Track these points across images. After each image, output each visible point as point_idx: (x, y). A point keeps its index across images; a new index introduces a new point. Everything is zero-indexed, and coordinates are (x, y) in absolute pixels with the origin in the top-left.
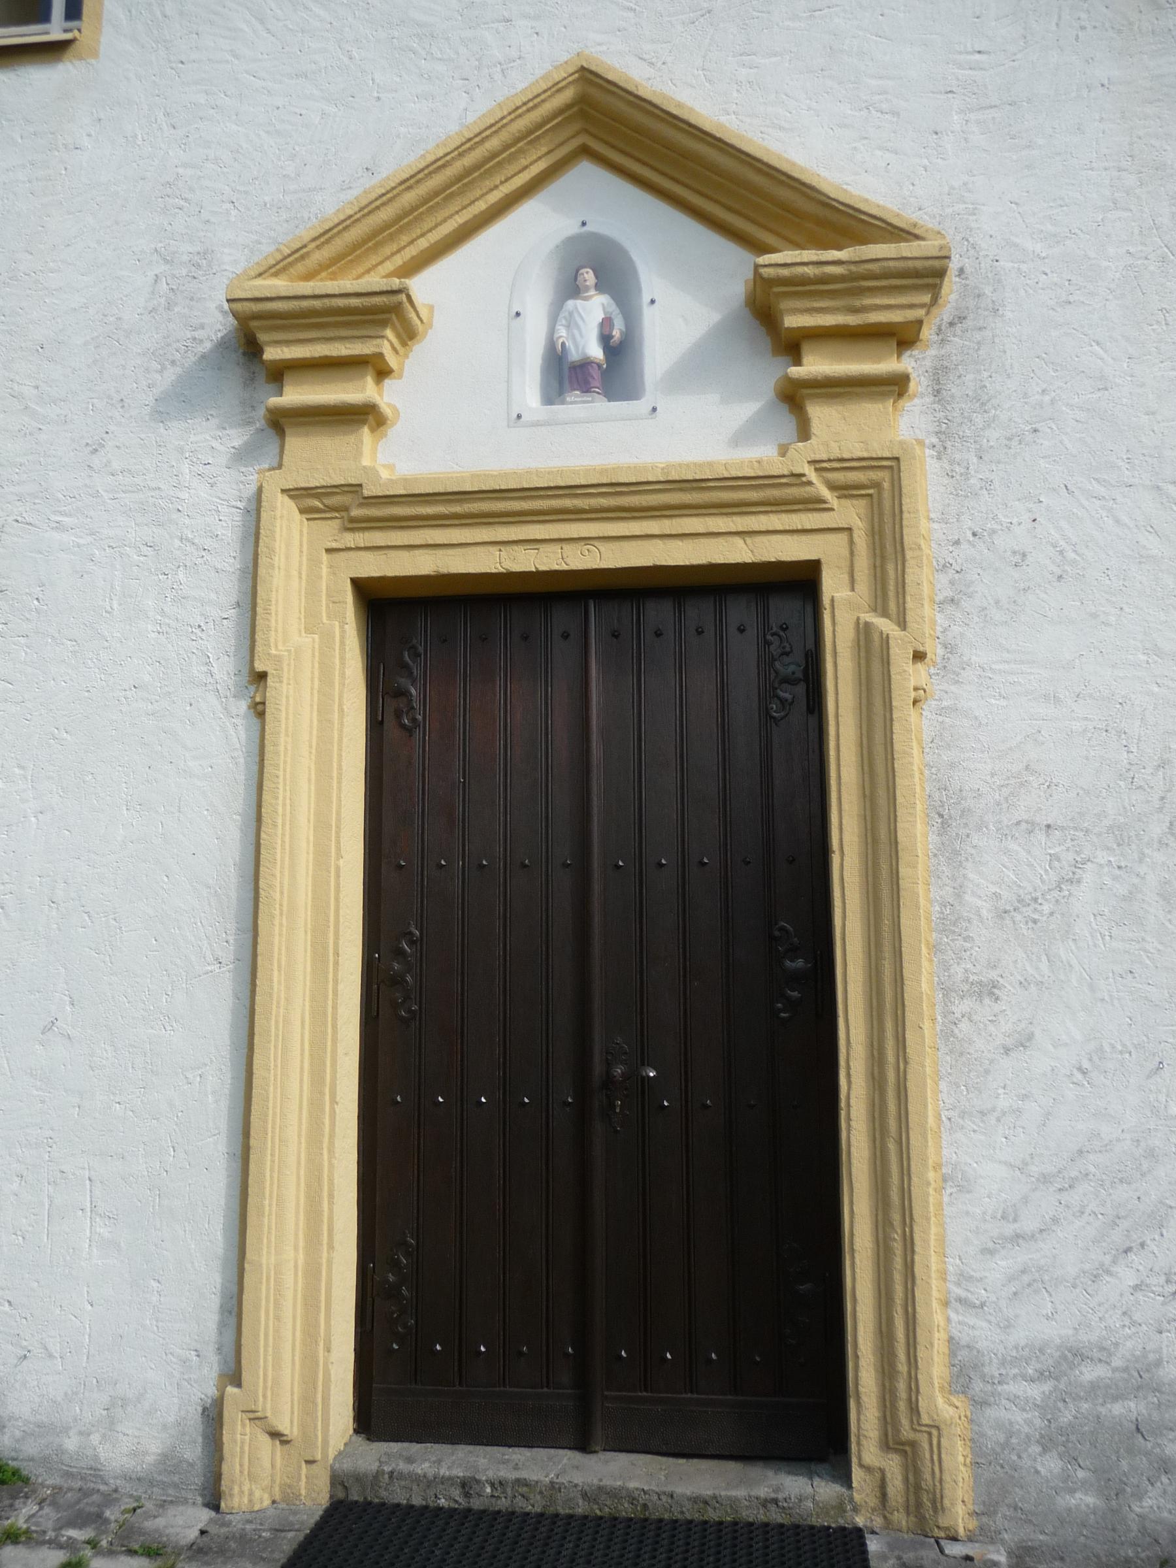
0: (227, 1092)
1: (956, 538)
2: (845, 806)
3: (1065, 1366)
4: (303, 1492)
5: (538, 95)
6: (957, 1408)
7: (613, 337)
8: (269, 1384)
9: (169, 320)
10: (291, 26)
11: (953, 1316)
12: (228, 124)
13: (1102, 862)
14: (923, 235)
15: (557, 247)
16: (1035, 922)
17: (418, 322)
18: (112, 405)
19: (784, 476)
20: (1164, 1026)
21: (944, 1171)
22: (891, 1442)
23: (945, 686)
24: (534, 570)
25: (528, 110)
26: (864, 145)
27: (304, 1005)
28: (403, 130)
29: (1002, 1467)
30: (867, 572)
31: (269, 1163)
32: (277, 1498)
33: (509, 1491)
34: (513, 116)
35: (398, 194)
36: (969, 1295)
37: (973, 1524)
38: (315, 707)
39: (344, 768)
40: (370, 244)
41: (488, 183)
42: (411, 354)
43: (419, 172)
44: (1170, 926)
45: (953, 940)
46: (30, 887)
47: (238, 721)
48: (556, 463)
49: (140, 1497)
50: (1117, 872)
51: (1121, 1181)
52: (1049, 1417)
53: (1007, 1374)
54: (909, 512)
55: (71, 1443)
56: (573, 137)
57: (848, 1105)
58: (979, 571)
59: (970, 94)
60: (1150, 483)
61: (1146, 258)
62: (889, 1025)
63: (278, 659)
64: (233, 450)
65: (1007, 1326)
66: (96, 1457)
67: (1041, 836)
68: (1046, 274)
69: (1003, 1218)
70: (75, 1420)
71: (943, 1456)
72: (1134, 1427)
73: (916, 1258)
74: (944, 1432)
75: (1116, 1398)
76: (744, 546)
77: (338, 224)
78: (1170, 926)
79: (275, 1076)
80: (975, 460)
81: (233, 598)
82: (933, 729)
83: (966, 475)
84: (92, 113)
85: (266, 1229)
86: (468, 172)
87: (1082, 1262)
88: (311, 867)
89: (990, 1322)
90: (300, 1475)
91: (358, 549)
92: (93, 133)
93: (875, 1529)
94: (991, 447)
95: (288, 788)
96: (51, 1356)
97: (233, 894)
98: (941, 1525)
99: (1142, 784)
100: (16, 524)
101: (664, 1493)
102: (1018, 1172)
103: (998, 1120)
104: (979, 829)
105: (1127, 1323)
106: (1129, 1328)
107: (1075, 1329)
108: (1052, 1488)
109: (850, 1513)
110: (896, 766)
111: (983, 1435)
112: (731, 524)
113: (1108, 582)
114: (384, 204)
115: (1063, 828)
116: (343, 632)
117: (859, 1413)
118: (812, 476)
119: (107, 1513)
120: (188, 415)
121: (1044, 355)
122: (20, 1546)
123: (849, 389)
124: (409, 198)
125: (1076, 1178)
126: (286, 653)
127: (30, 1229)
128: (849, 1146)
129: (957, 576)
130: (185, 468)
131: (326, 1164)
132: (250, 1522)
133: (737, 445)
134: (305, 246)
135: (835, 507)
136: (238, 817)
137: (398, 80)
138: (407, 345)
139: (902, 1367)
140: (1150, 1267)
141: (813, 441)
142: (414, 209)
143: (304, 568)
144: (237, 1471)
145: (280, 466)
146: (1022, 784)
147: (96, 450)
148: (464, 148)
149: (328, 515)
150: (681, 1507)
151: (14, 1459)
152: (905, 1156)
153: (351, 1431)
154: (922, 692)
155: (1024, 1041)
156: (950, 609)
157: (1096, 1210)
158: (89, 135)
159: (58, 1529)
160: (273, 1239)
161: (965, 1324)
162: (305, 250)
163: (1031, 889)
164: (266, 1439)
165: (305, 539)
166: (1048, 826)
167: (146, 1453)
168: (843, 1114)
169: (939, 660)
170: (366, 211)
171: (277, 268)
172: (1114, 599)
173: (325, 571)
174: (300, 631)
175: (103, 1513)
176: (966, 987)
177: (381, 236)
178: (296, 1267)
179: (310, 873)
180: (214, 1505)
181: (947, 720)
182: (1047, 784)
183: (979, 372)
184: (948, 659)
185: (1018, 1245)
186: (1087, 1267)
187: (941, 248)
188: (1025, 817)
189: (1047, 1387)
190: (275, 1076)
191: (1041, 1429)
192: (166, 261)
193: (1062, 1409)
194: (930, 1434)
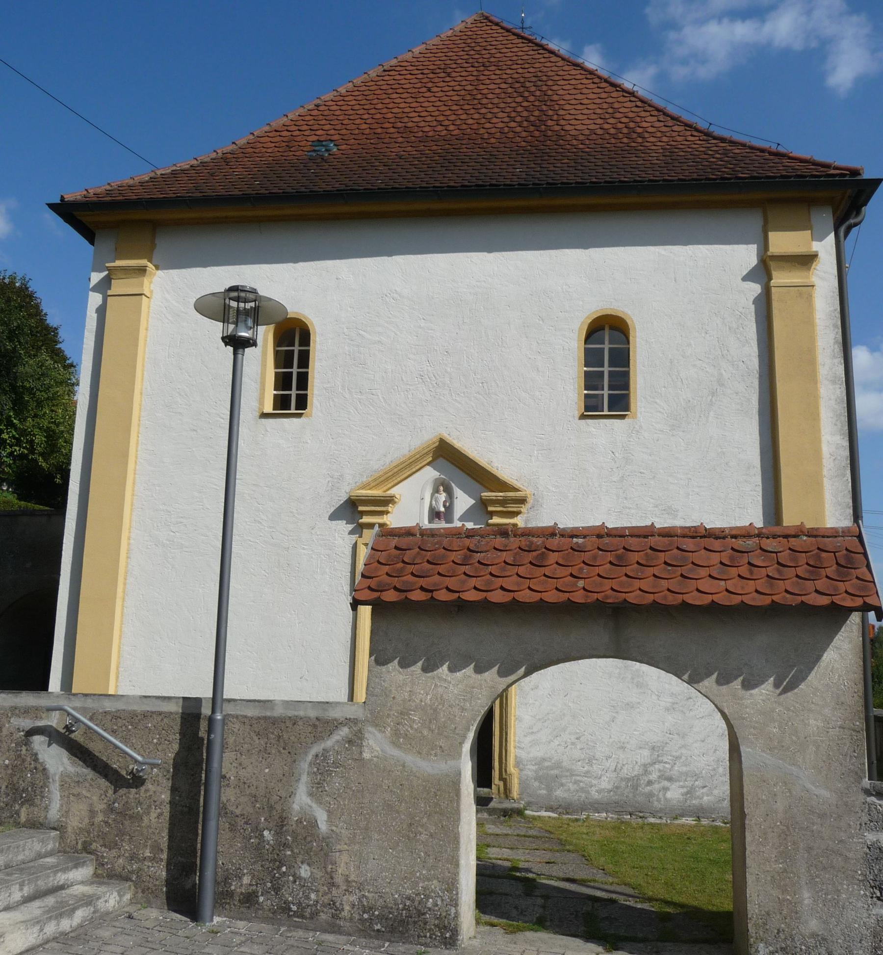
37: (518, 796)
65: (529, 753)
124: (396, 470)
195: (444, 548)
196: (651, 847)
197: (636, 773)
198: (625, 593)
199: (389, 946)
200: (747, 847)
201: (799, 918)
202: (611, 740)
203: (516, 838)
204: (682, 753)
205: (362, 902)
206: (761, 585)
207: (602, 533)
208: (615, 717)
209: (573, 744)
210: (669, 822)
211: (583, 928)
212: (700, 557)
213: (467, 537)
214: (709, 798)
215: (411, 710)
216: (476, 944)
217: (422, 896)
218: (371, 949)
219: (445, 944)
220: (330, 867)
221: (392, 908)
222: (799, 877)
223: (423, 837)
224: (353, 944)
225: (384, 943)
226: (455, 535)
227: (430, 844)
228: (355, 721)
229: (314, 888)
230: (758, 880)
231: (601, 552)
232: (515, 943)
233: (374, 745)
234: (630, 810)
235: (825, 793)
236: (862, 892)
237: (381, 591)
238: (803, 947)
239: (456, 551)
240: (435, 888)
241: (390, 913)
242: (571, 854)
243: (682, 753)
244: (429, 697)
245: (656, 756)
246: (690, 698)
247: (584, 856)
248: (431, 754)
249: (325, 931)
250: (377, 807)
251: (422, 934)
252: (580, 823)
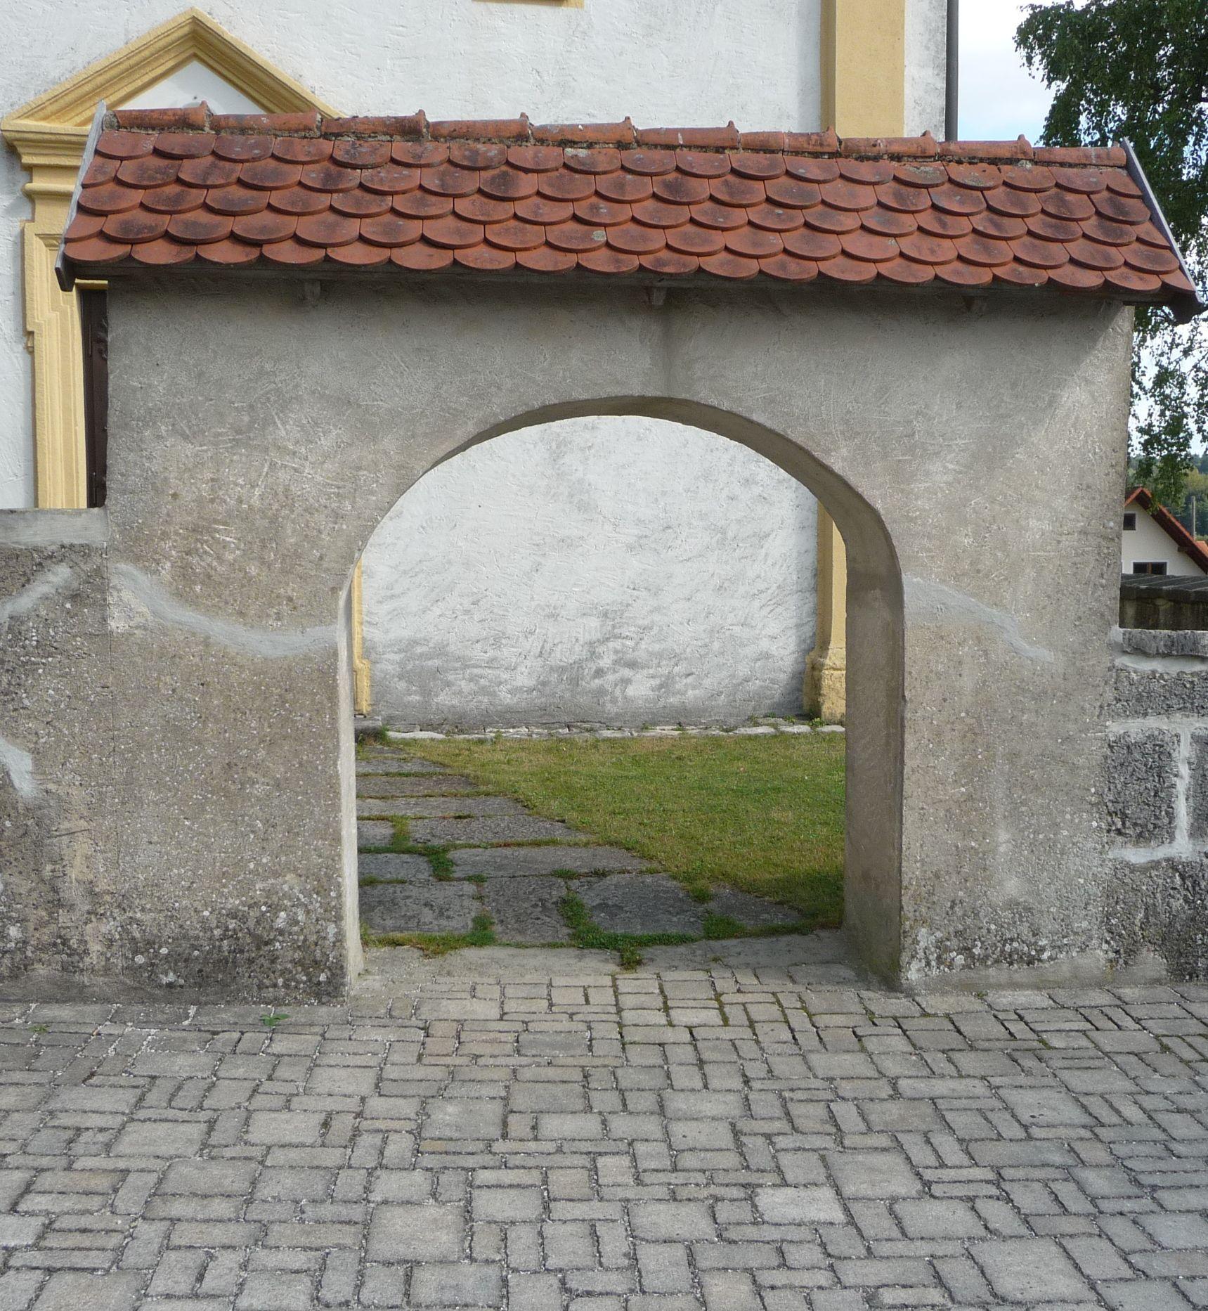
37: (369, 709)
63: (39, 325)
65: (387, 632)
81: (11, 290)
86: (131, 67)
116: (72, 310)
124: (100, 80)
145: (33, 220)
189: (402, 655)
195: (273, 156)
196: (627, 777)
197: (576, 657)
198: (699, 255)
199: (197, 1013)
200: (906, 760)
201: (989, 878)
202: (533, 604)
203: (384, 779)
204: (653, 622)
205: (128, 932)
206: (967, 247)
207: (629, 137)
208: (540, 564)
209: (467, 612)
210: (635, 734)
211: (566, 931)
212: (837, 192)
213: (326, 136)
214: (697, 692)
215: (218, 522)
216: (377, 985)
217: (264, 908)
218: (161, 1025)
219: (318, 996)
220: (49, 867)
221: (197, 938)
222: (993, 807)
223: (259, 790)
224: (116, 1018)
225: (186, 1010)
226: (297, 131)
227: (276, 802)
228: (85, 551)
229: (14, 914)
230: (922, 818)
231: (629, 177)
232: (449, 974)
233: (134, 603)
234: (566, 719)
235: (1046, 655)
236: (1095, 824)
237: (133, 243)
238: (993, 927)
239: (303, 163)
240: (291, 888)
241: (194, 948)
242: (491, 800)
243: (653, 622)
244: (257, 492)
245: (609, 628)
246: (669, 527)
247: (517, 800)
248: (268, 616)
249: (47, 1000)
250: (150, 735)
251: (267, 982)
252: (488, 746)
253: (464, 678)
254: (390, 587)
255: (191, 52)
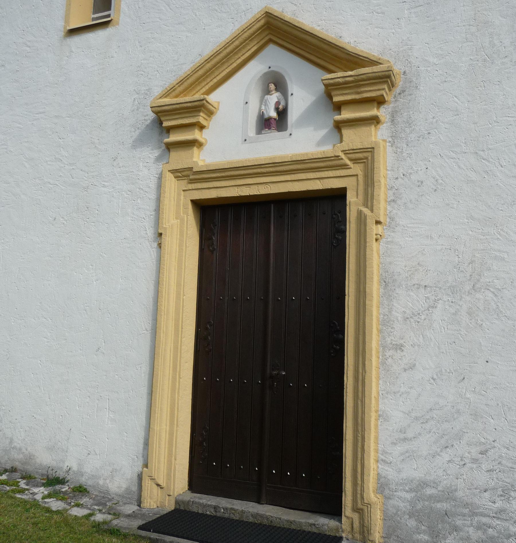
0: (148, 373)
1: (397, 177)
2: (350, 278)
3: (420, 488)
4: (167, 505)
5: (251, 24)
6: (379, 499)
7: (279, 108)
8: (156, 468)
9: (138, 114)
10: (178, 6)
11: (380, 466)
12: (157, 44)
13: (446, 300)
14: (382, 63)
15: (261, 77)
16: (418, 322)
17: (213, 109)
18: (120, 144)
19: (332, 157)
20: (466, 363)
21: (379, 413)
22: (356, 509)
23: (389, 233)
24: (249, 195)
25: (248, 30)
26: (370, 27)
27: (171, 345)
28: (212, 39)
29: (394, 522)
30: (362, 191)
31: (158, 396)
32: (159, 506)
33: (229, 511)
34: (243, 32)
35: (205, 65)
36: (386, 459)
38: (178, 244)
39: (186, 265)
40: (197, 83)
41: (237, 57)
42: (212, 120)
43: (211, 56)
44: (471, 325)
45: (387, 328)
46: (93, 305)
47: (154, 250)
48: (257, 156)
49: (119, 501)
50: (451, 304)
51: (446, 421)
52: (413, 506)
53: (398, 488)
54: (377, 168)
55: (101, 482)
56: (266, 36)
57: (347, 388)
58: (405, 189)
59: (412, 2)
60: (473, 151)
61: (478, 61)
62: (361, 359)
63: (165, 229)
64: (155, 157)
65: (399, 471)
66: (108, 487)
67: (423, 290)
68: (437, 71)
69: (400, 432)
70: (102, 475)
71: (371, 515)
72: (445, 513)
73: (365, 443)
74: (372, 506)
75: (438, 502)
76: (320, 183)
77: (185, 78)
78: (471, 325)
79: (161, 368)
80: (405, 146)
81: (154, 209)
82: (383, 249)
83: (402, 152)
84: (117, 44)
85: (156, 418)
86: (228, 54)
87: (429, 450)
88: (175, 299)
89: (393, 469)
90: (166, 500)
91: (193, 189)
92: (117, 51)
93: (349, 539)
94: (412, 141)
95: (167, 272)
96: (96, 454)
97: (151, 308)
98: (370, 539)
99: (463, 270)
100: (92, 186)
101: (278, 518)
102: (407, 415)
103: (400, 396)
104: (399, 287)
105: (445, 474)
106: (446, 476)
107: (425, 475)
108: (412, 531)
109: (341, 532)
110: (367, 263)
111: (388, 509)
112: (315, 175)
113: (454, 191)
114: (200, 69)
115: (431, 287)
117: (345, 497)
118: (343, 156)
119: (107, 503)
120: (142, 146)
121: (435, 103)
122: (79, 508)
123: (357, 123)
124: (209, 66)
125: (429, 419)
126: (168, 226)
127: (92, 414)
128: (346, 402)
129: (396, 191)
130: (141, 164)
131: (177, 398)
132: (148, 511)
133: (319, 146)
134: (174, 86)
135: (352, 167)
136: (154, 282)
137: (211, 21)
138: (211, 117)
139: (359, 482)
140: (455, 454)
141: (343, 143)
142: (210, 69)
143: (176, 197)
144: (146, 495)
146: (416, 270)
147: (115, 160)
148: (226, 46)
149: (184, 178)
150: (283, 523)
151: (86, 486)
152: (363, 406)
153: (187, 489)
154: (379, 236)
155: (412, 367)
156: (392, 204)
157: (435, 431)
158: (116, 52)
159: (91, 505)
160: (159, 421)
161: (384, 469)
162: (174, 88)
163: (418, 310)
164: (156, 486)
165: (176, 187)
166: (425, 286)
167: (121, 487)
168: (345, 390)
169: (387, 224)
170: (194, 72)
171: (166, 95)
172: (456, 198)
173: (182, 198)
174: (174, 219)
175: (106, 503)
176: (391, 346)
177: (200, 80)
178: (166, 431)
179: (175, 301)
180: (139, 506)
181: (389, 246)
182: (426, 270)
183: (409, 112)
184: (391, 223)
185: (405, 442)
186: (431, 452)
187: (388, 67)
188: (417, 283)
189: (413, 495)
190: (161, 368)
191: (409, 510)
192: (137, 94)
193: (418, 503)
194: (367, 506)
209: (475, 461)
253: (472, 525)
254: (402, 431)
255: (267, 38)
